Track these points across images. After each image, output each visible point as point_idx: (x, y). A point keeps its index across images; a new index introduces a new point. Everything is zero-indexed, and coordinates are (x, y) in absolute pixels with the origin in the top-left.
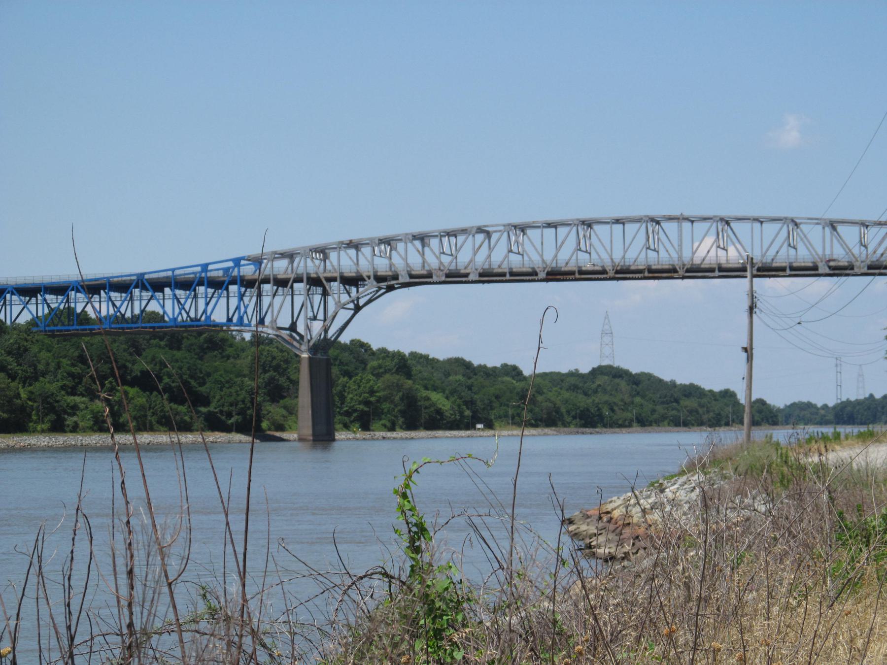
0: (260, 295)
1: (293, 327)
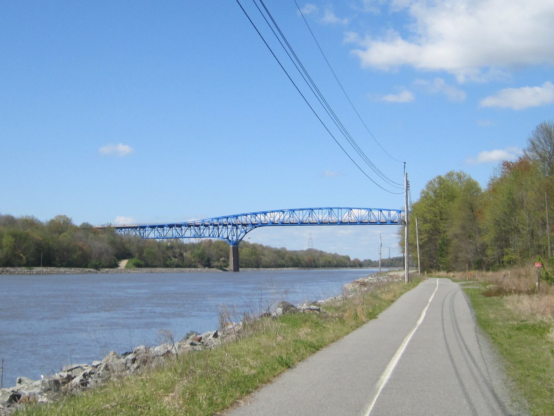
0: (218, 229)
1: (228, 238)
